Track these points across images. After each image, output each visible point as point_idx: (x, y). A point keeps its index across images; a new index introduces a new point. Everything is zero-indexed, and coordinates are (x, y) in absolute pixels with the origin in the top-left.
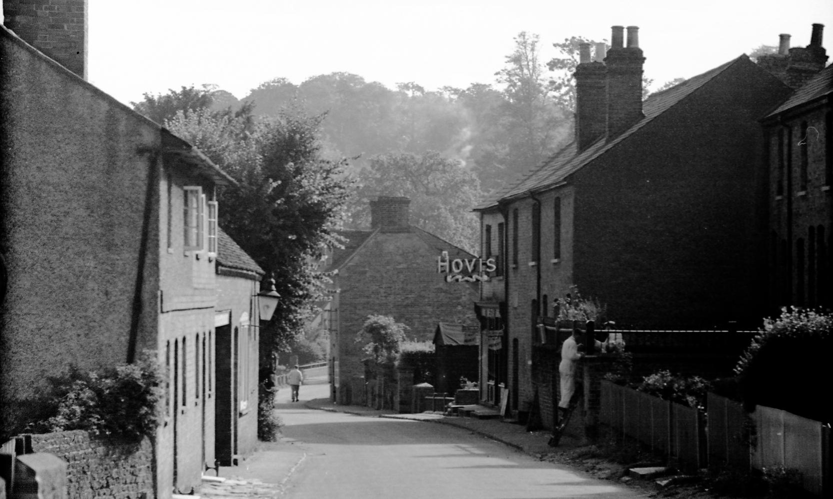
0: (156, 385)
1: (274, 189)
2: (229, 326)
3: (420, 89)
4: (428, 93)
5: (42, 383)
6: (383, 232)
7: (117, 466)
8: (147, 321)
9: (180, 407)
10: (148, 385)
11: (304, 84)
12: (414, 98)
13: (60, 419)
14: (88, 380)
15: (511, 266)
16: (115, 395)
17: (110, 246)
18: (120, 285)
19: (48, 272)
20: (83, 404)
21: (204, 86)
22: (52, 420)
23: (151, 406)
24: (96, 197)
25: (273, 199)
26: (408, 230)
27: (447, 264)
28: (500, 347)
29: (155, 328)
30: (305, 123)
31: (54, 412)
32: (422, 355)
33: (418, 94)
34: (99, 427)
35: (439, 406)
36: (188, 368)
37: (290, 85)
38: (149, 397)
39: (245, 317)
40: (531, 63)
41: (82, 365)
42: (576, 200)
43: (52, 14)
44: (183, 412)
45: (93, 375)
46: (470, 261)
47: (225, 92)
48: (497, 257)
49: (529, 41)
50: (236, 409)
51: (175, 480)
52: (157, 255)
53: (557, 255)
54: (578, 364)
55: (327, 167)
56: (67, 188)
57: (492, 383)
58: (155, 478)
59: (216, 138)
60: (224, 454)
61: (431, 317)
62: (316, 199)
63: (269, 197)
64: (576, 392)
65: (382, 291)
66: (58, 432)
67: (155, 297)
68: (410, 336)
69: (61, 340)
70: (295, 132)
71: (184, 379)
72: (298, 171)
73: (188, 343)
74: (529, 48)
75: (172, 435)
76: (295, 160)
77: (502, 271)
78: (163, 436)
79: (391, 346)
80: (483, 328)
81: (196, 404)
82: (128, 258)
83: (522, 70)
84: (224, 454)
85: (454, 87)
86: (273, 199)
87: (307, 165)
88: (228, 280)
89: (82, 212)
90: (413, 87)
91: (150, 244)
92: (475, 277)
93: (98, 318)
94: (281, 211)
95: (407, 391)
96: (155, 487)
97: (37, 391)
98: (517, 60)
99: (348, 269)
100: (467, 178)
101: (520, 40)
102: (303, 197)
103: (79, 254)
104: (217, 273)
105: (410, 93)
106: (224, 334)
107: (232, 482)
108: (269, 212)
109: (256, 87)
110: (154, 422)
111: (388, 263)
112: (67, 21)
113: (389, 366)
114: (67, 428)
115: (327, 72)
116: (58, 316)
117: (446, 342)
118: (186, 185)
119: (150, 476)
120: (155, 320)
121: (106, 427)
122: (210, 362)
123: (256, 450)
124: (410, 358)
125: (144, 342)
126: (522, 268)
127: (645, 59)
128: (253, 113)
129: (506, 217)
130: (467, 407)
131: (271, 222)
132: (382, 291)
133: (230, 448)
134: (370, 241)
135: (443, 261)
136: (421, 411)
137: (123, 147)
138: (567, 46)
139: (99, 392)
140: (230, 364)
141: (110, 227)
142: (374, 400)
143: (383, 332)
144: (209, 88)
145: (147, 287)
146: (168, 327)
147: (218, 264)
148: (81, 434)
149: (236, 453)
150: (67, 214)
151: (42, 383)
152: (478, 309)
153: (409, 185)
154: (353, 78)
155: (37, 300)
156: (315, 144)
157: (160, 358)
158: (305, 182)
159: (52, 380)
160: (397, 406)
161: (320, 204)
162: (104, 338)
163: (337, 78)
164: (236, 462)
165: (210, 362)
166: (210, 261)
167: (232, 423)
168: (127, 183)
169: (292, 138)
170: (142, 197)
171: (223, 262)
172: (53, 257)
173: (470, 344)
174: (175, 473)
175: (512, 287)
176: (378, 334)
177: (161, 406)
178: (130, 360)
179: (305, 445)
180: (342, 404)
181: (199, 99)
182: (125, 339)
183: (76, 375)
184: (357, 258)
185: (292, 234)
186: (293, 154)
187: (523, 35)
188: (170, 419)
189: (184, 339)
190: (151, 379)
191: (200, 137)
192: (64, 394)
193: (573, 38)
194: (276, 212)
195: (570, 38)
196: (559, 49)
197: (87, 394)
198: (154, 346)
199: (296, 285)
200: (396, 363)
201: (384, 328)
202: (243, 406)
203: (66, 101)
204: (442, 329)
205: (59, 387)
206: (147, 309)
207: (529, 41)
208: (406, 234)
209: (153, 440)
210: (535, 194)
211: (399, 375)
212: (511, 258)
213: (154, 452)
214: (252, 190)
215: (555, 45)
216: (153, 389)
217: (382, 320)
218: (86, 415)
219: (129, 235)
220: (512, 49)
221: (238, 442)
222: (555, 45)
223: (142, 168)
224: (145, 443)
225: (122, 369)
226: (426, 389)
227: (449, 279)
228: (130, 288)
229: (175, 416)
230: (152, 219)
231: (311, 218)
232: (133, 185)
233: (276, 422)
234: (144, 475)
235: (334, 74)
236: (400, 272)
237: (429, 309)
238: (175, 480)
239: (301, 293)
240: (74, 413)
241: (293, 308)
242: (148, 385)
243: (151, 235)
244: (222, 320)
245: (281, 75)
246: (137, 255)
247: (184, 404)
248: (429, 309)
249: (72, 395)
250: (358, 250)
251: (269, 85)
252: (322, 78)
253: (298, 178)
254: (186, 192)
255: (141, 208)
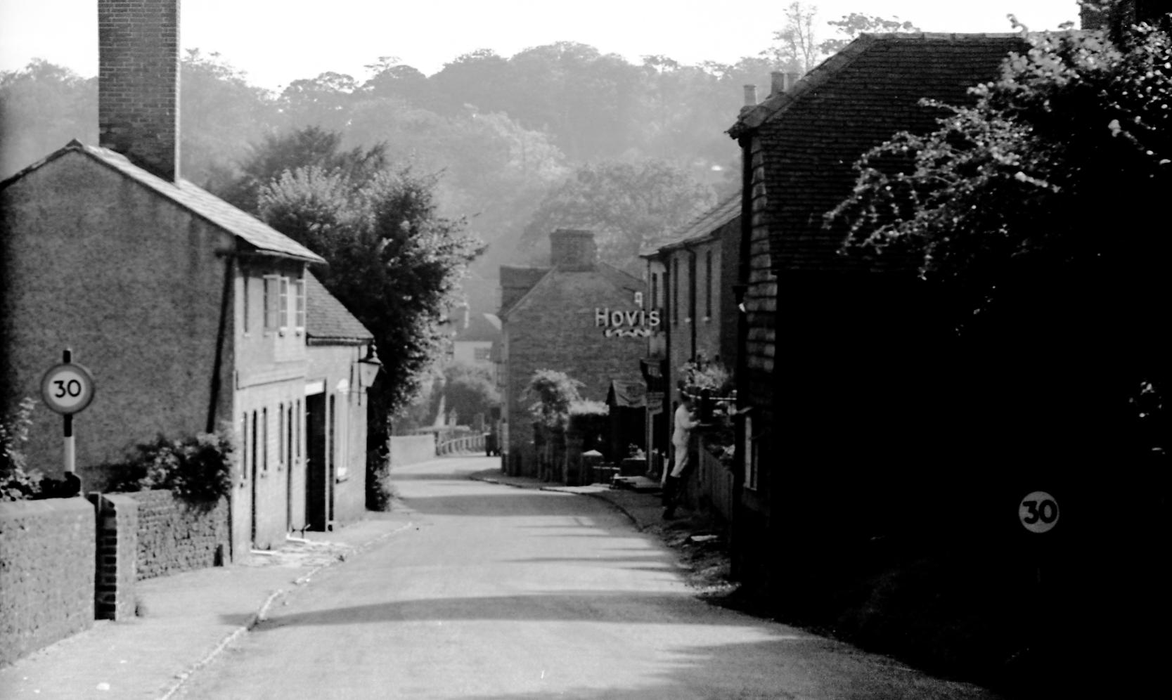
0: (230, 451)
1: (386, 248)
2: (323, 395)
3: (671, 63)
4: (685, 69)
5: (132, 450)
6: (562, 271)
7: (196, 520)
8: (224, 396)
9: (260, 470)
10: (224, 451)
11: (518, 58)
12: (665, 75)
13: (148, 480)
14: (173, 447)
15: (672, 321)
16: (195, 458)
17: (192, 334)
18: (201, 366)
19: (137, 356)
20: (167, 467)
21: (382, 59)
22: (141, 481)
23: (226, 469)
24: (180, 292)
25: (386, 258)
26: (590, 268)
27: (605, 317)
28: (660, 411)
29: (231, 401)
30: (422, 181)
31: (143, 474)
32: (594, 418)
33: (669, 69)
34: (181, 486)
35: (604, 478)
36: (270, 436)
37: (497, 58)
38: (225, 462)
39: (343, 386)
40: (806, 41)
41: (169, 434)
42: (723, 255)
43: (147, 126)
44: (262, 476)
45: (178, 444)
46: (631, 315)
47: (410, 68)
48: (661, 311)
49: (804, 14)
50: (331, 475)
51: (253, 537)
52: (232, 340)
53: (709, 314)
54: (693, 433)
55: (446, 225)
56: (155, 285)
57: (656, 452)
58: (230, 532)
59: (328, 197)
60: (317, 518)
61: (618, 371)
62: (432, 258)
63: (383, 256)
64: (689, 462)
65: (560, 339)
66: (146, 491)
67: (231, 376)
68: (584, 394)
69: (149, 414)
70: (411, 190)
71: (265, 447)
72: (413, 231)
73: (269, 413)
74: (803, 22)
75: (250, 495)
76: (410, 218)
77: (665, 327)
78: (240, 498)
79: (562, 406)
80: (650, 389)
81: (279, 469)
82: (206, 345)
83: (794, 48)
84: (317, 518)
85: (718, 62)
86: (386, 258)
87: (424, 224)
88: (322, 351)
89: (169, 306)
90: (664, 61)
91: (227, 332)
92: (637, 331)
93: (181, 394)
94: (396, 270)
95: (575, 459)
96: (230, 540)
97: (128, 456)
98: (788, 36)
99: (520, 314)
100: (701, 192)
101: (793, 12)
102: (420, 256)
103: (165, 341)
104: (307, 344)
105: (659, 68)
106: (316, 404)
107: (314, 544)
108: (383, 272)
109: (450, 61)
110: (229, 483)
111: (567, 307)
112: (159, 131)
113: (558, 430)
114: (154, 488)
115: (548, 41)
116: (147, 393)
117: (620, 402)
118: (266, 273)
119: (227, 529)
120: (231, 394)
121: (187, 487)
122: (298, 430)
123: (361, 519)
124: (579, 420)
125: (222, 414)
126: (681, 323)
127: (743, 133)
128: (386, 152)
129: (668, 268)
130: (631, 479)
131: (382, 283)
132: (560, 339)
133: (324, 513)
134: (546, 282)
135: (601, 313)
136: (588, 484)
137: (204, 253)
138: (846, 24)
139: (180, 457)
140: (323, 431)
141: (192, 318)
142: (543, 470)
143: (552, 390)
144: (387, 61)
145: (224, 369)
146: (243, 402)
147: (308, 336)
148: (166, 494)
149: (331, 519)
150: (154, 307)
151: (132, 450)
152: (644, 367)
153: (628, 200)
154: (582, 49)
155: (127, 380)
156: (433, 202)
157: (236, 428)
158: (421, 242)
159: (142, 448)
160: (566, 479)
161: (437, 264)
162: (187, 412)
163: (563, 50)
164: (330, 528)
165: (298, 430)
166: (298, 335)
167: (327, 489)
168: (207, 281)
169: (407, 196)
170: (220, 293)
171: (313, 333)
172: (143, 343)
173: (635, 406)
174: (254, 530)
175: (673, 343)
176: (548, 394)
177: (237, 469)
178: (210, 429)
179: (421, 515)
180: (511, 475)
181: (326, 139)
182: (205, 412)
183: (162, 443)
184: (529, 301)
185: (407, 294)
186: (408, 212)
187: (795, 6)
188: (248, 482)
189: (265, 411)
190: (226, 447)
191: (309, 196)
192: (151, 460)
193: (853, 15)
194: (391, 272)
195: (848, 15)
196: (836, 27)
197: (171, 460)
198: (230, 419)
199: (413, 347)
200: (566, 427)
201: (553, 385)
202: (340, 472)
203: (154, 214)
204: (615, 387)
205: (149, 452)
206: (224, 386)
207: (804, 14)
208: (590, 274)
209: (229, 498)
210: (689, 246)
211: (567, 441)
212: (672, 312)
213: (230, 510)
214: (364, 250)
215: (830, 23)
216: (228, 455)
217: (552, 376)
218: (172, 475)
219: (208, 325)
220: (782, 24)
221: (335, 508)
222: (830, 23)
223: (219, 268)
224: (222, 501)
225: (203, 438)
226: (594, 458)
227: (608, 333)
228: (210, 369)
229: (254, 479)
230: (228, 310)
231: (427, 281)
232: (212, 283)
233: (390, 491)
234: (221, 529)
235: (558, 44)
236: (581, 317)
237: (616, 362)
238: (253, 537)
239: (417, 355)
240: (159, 475)
241: (409, 371)
242: (224, 451)
243: (228, 324)
244: (316, 388)
245: (484, 45)
246: (215, 341)
247: (265, 468)
248: (616, 362)
249: (158, 460)
250: (531, 292)
251: (469, 58)
252: (542, 50)
253: (414, 237)
254: (266, 282)
255: (219, 300)
